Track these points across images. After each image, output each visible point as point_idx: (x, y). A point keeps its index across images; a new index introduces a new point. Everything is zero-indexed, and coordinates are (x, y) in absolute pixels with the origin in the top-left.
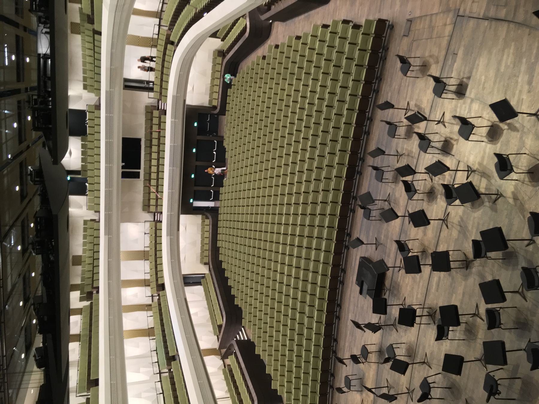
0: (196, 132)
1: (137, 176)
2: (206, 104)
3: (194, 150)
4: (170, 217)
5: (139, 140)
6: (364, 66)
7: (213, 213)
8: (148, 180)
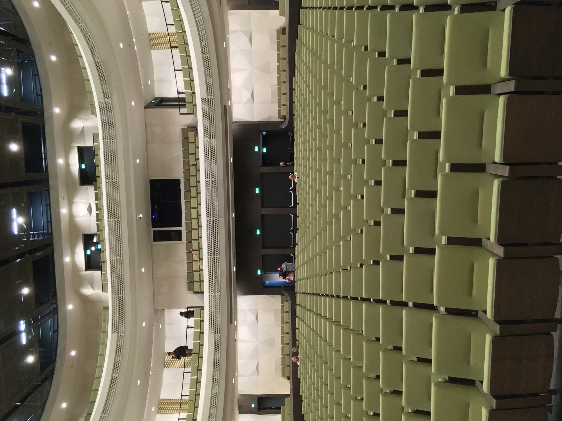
0: (260, 162)
1: (177, 236)
2: (275, 118)
3: (257, 191)
4: (215, 301)
5: (178, 182)
6: (491, 169)
7: (288, 291)
8: (190, 242)
